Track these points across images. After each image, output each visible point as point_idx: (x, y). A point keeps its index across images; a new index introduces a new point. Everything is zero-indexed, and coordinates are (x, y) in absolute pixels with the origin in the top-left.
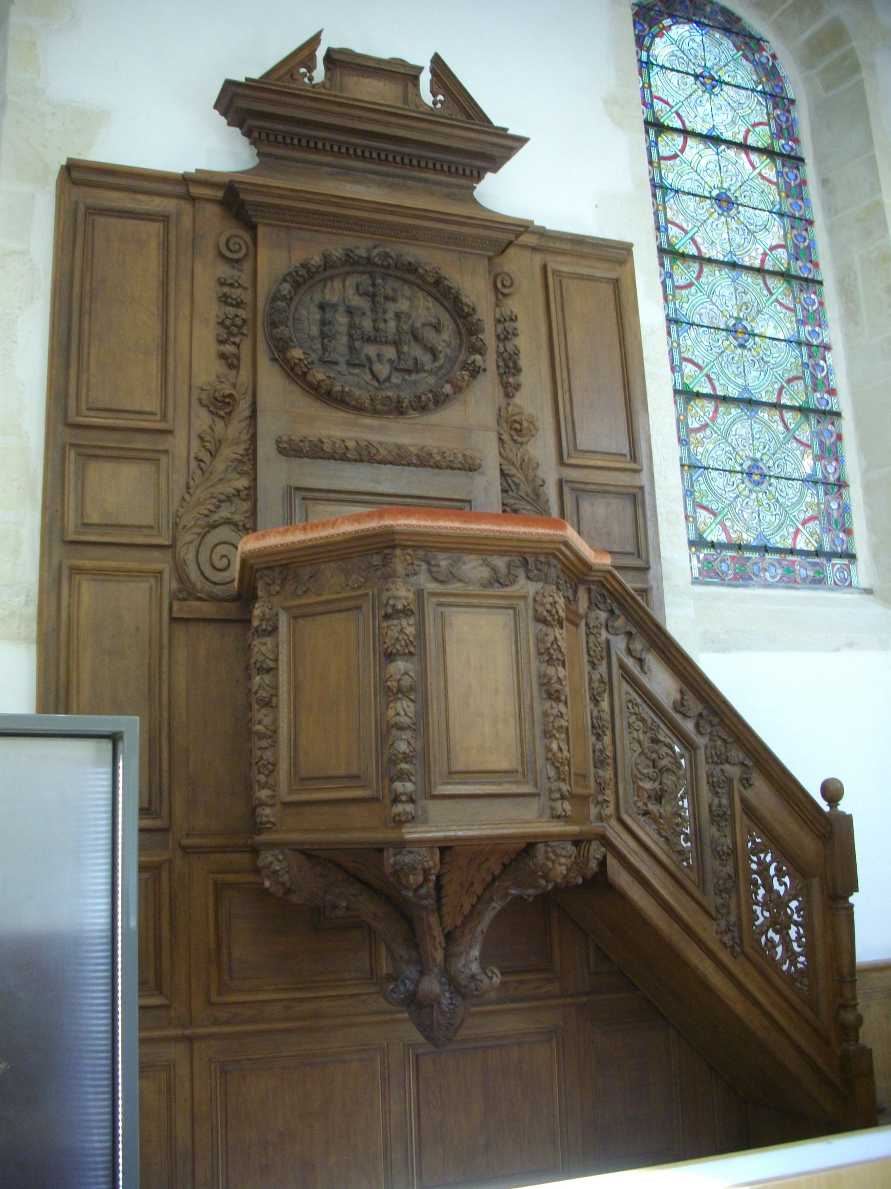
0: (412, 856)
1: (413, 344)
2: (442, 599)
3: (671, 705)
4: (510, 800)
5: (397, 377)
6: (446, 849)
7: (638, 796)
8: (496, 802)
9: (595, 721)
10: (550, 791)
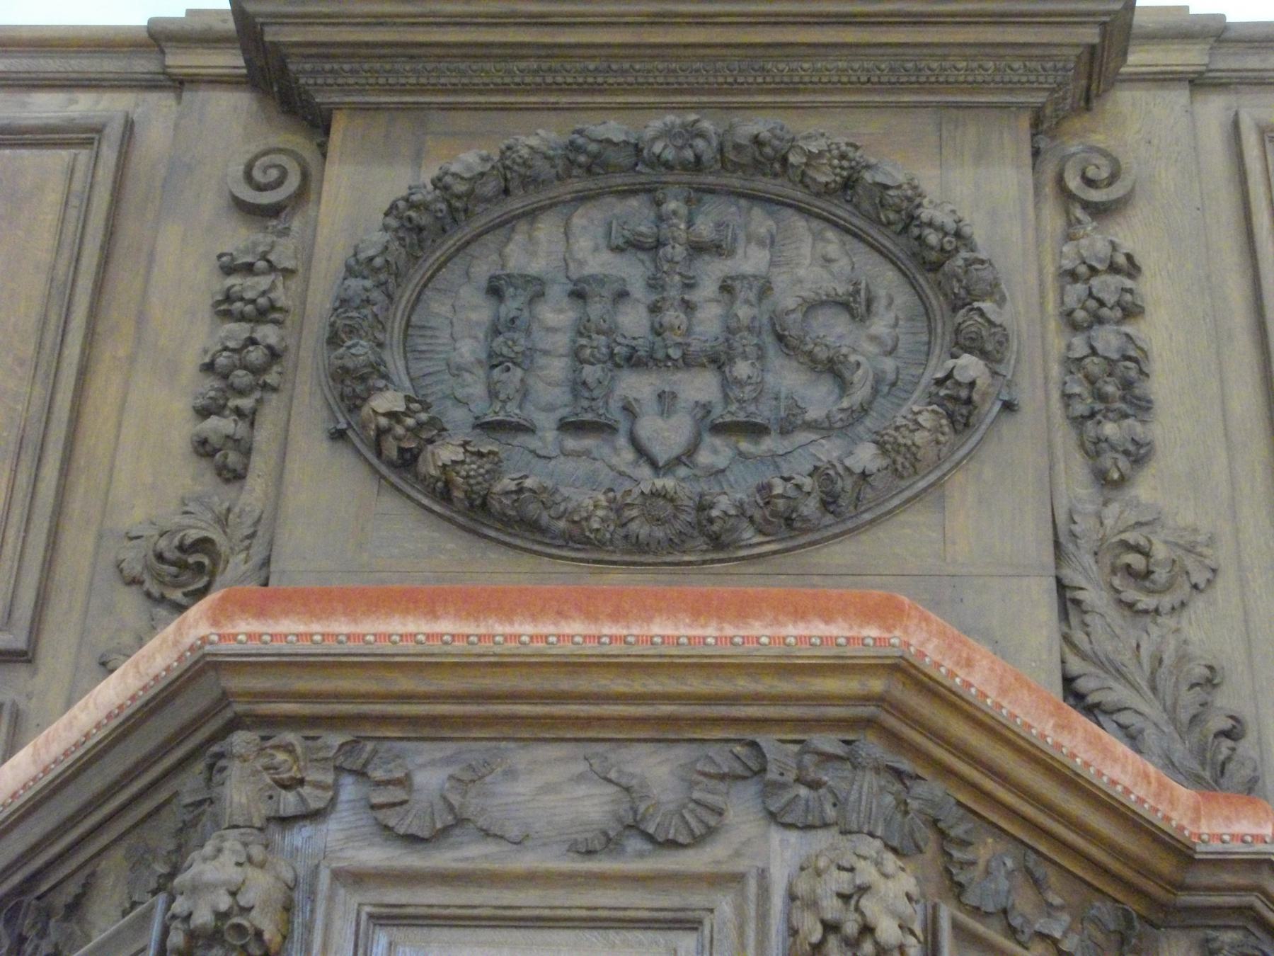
1: (775, 358)
2: (395, 896)
5: (715, 451)
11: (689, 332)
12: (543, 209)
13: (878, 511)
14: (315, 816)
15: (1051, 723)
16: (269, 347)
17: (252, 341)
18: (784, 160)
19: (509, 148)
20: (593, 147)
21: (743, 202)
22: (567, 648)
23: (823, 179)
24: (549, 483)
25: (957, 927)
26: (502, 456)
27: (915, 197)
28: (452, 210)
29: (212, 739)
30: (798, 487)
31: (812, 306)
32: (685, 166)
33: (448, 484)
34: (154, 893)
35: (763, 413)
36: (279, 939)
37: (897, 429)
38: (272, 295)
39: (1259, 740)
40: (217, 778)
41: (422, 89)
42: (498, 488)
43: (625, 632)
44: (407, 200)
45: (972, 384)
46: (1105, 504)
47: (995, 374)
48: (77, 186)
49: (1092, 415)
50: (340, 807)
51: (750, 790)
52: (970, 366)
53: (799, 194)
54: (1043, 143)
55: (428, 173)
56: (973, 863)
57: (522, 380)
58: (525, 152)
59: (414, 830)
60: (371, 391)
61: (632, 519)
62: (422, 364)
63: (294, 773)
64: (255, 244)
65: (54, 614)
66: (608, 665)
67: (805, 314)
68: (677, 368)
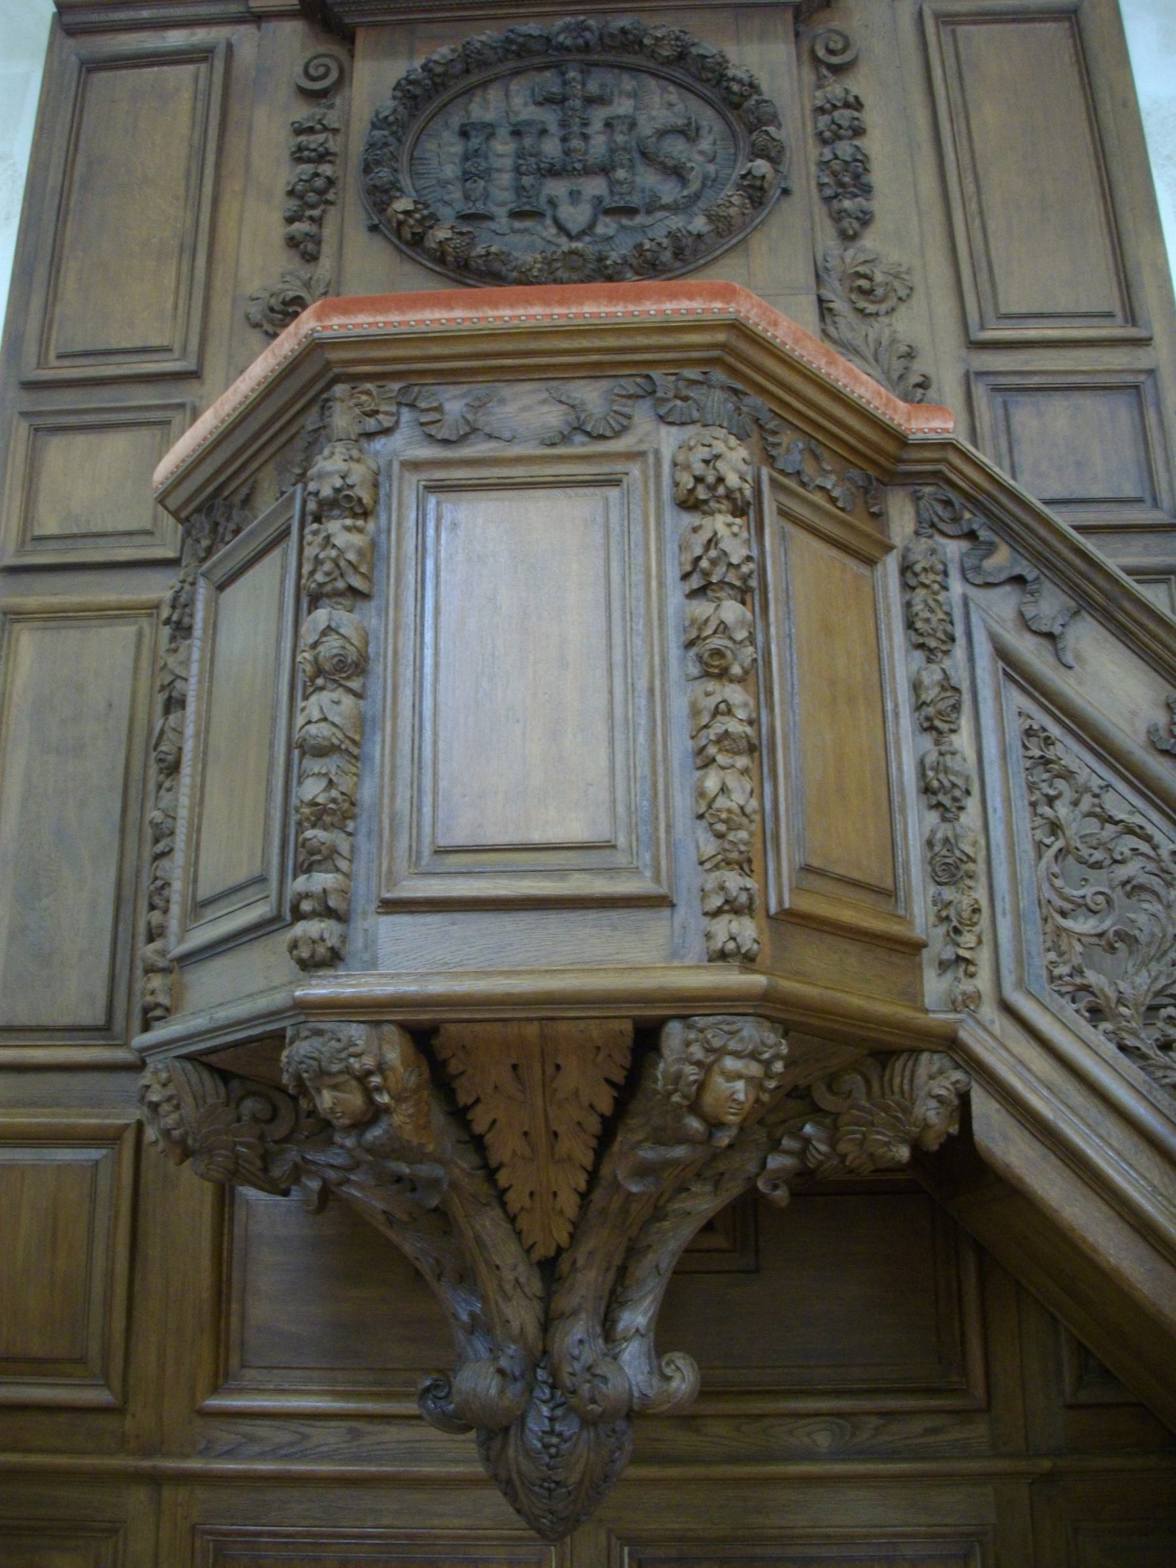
0: (317, 1042)
1: (641, 168)
2: (439, 474)
3: (1142, 737)
4: (592, 915)
5: (606, 226)
6: (429, 1034)
7: (1061, 954)
8: (553, 921)
9: (930, 774)
10: (704, 894)
11: (586, 153)
12: (491, 81)
13: (709, 258)
14: (387, 432)
15: (824, 361)
16: (328, 178)
17: (317, 175)
18: (641, 43)
19: (468, 43)
20: (521, 40)
21: (616, 71)
22: (532, 323)
23: (666, 54)
24: (505, 249)
25: (772, 480)
26: (477, 234)
27: (723, 62)
28: (435, 84)
29: (322, 391)
30: (659, 244)
31: (662, 134)
32: (579, 50)
33: (443, 253)
34: (294, 485)
35: (636, 200)
36: (371, 503)
37: (719, 206)
38: (327, 145)
39: (939, 389)
40: (327, 413)
41: (409, 10)
42: (474, 254)
43: (566, 311)
44: (406, 79)
45: (763, 177)
46: (845, 250)
47: (777, 171)
48: (201, 86)
49: (836, 196)
50: (402, 426)
51: (647, 403)
52: (761, 166)
53: (651, 64)
54: (802, 29)
55: (418, 63)
56: (779, 444)
57: (485, 188)
58: (478, 45)
59: (445, 437)
60: (392, 199)
61: (558, 269)
62: (422, 181)
63: (372, 407)
64: (314, 115)
65: (211, 350)
66: (557, 332)
67: (658, 138)
68: (580, 175)
